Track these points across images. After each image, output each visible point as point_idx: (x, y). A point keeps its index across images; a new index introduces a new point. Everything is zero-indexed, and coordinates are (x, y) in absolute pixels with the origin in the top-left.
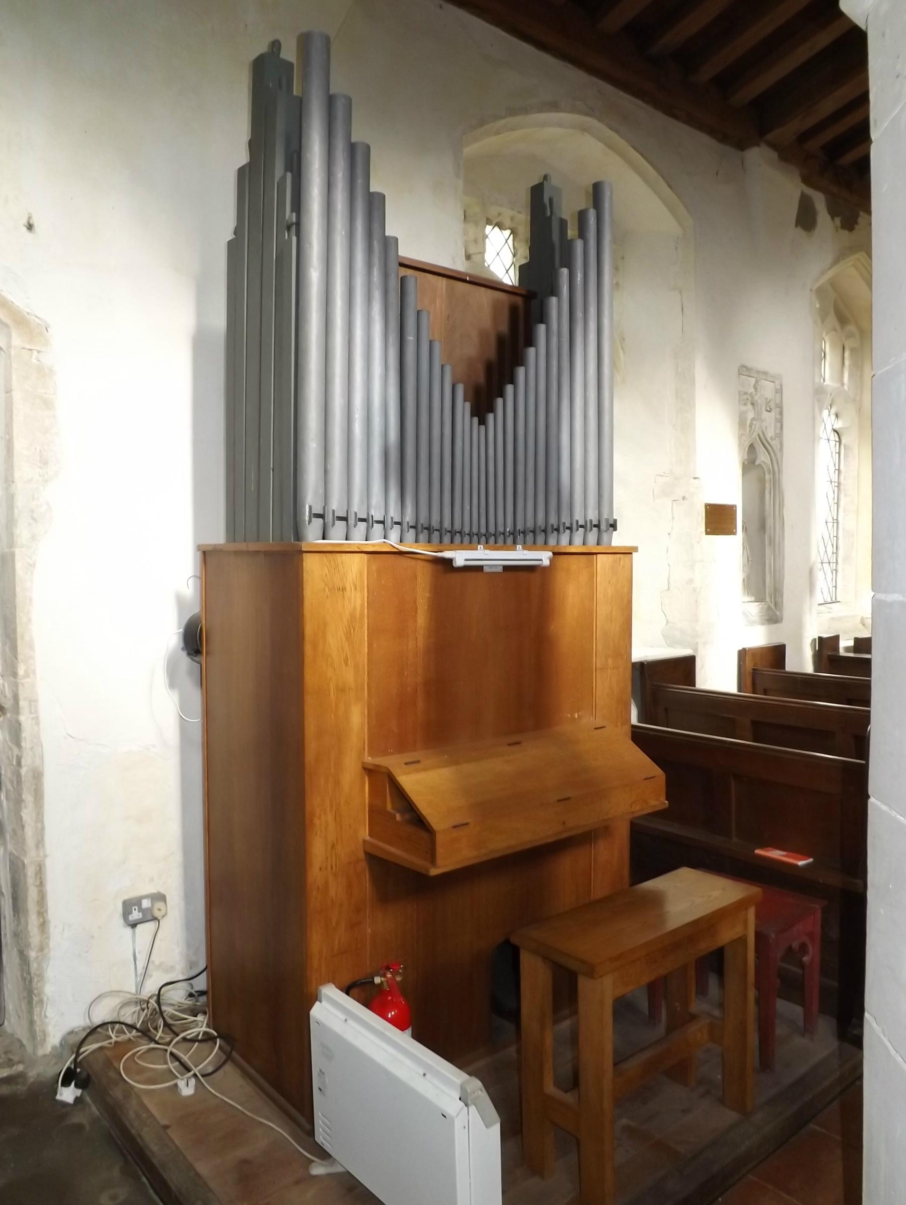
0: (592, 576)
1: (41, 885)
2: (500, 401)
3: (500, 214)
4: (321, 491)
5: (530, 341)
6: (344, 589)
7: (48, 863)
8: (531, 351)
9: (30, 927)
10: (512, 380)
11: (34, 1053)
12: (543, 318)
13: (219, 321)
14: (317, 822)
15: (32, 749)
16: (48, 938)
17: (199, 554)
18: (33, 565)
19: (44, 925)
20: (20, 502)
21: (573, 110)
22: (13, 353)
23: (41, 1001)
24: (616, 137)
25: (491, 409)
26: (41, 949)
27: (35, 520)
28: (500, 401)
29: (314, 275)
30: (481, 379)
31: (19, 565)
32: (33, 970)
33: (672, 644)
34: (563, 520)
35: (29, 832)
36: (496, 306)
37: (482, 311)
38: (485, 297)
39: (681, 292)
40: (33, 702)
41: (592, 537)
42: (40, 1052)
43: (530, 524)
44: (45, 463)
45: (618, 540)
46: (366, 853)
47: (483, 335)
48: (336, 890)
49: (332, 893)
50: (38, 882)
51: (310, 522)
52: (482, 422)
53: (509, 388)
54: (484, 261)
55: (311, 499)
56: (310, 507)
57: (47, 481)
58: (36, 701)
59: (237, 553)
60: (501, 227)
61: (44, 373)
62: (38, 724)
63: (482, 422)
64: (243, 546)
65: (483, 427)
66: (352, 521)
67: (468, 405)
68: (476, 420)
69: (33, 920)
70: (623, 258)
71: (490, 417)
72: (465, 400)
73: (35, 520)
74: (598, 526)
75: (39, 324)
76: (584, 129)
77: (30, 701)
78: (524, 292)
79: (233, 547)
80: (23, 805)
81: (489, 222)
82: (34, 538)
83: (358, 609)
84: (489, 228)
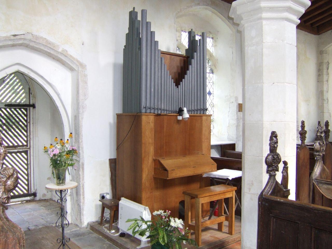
0: (202, 121)
1: (83, 189)
2: (181, 83)
3: (185, 29)
4: (145, 103)
5: (188, 69)
6: (149, 123)
7: (85, 184)
8: (188, 71)
9: (81, 198)
10: (184, 78)
11: (81, 226)
12: (191, 64)
13: (121, 60)
14: (144, 170)
15: (82, 158)
16: (84, 201)
17: (116, 116)
18: (83, 118)
19: (84, 198)
20: (80, 104)
21: (204, 5)
22: (79, 72)
23: (83, 215)
24: (214, 10)
25: (179, 84)
26: (83, 203)
27: (83, 108)
28: (181, 83)
29: (144, 59)
30: (177, 77)
31: (80, 118)
32: (81, 208)
33: (231, 140)
34: (195, 109)
35: (81, 177)
36: (181, 60)
37: (177, 62)
38: (178, 58)
39: (232, 48)
40: (82, 148)
41: (202, 112)
42: (83, 226)
43: (196, 108)
44: (85, 95)
45: (208, 113)
46: (153, 177)
47: (178, 67)
48: (147, 184)
49: (147, 185)
50: (83, 188)
51: (143, 109)
52: (178, 87)
53: (183, 80)
54: (181, 41)
55: (143, 104)
56: (143, 106)
57: (86, 100)
58: (83, 148)
59: (126, 115)
60: (185, 32)
61: (85, 76)
62: (83, 153)
63: (178, 87)
64: (127, 114)
65: (178, 88)
66: (151, 109)
67: (175, 84)
68: (176, 87)
69: (82, 197)
70: (217, 38)
71: (179, 86)
72: (174, 83)
73: (83, 108)
74: (194, 111)
75: (84, 65)
76: (206, 9)
77: (82, 148)
78: (186, 57)
79: (124, 114)
80: (80, 171)
81: (182, 31)
82: (83, 112)
83: (152, 127)
84: (182, 33)
